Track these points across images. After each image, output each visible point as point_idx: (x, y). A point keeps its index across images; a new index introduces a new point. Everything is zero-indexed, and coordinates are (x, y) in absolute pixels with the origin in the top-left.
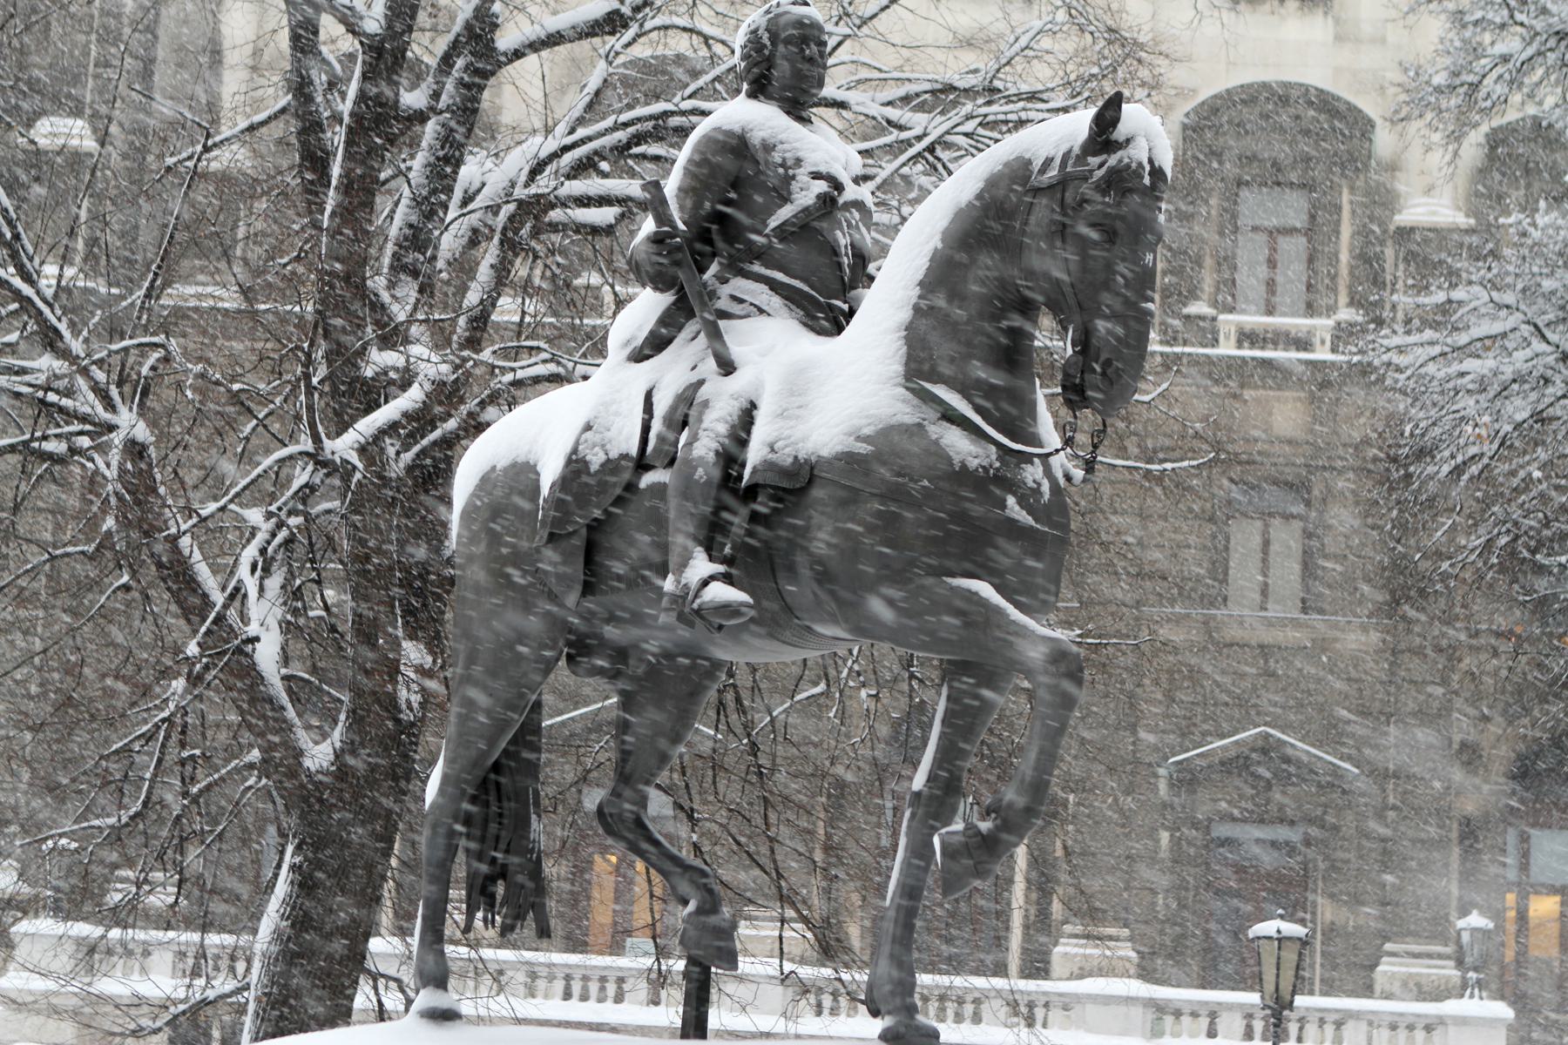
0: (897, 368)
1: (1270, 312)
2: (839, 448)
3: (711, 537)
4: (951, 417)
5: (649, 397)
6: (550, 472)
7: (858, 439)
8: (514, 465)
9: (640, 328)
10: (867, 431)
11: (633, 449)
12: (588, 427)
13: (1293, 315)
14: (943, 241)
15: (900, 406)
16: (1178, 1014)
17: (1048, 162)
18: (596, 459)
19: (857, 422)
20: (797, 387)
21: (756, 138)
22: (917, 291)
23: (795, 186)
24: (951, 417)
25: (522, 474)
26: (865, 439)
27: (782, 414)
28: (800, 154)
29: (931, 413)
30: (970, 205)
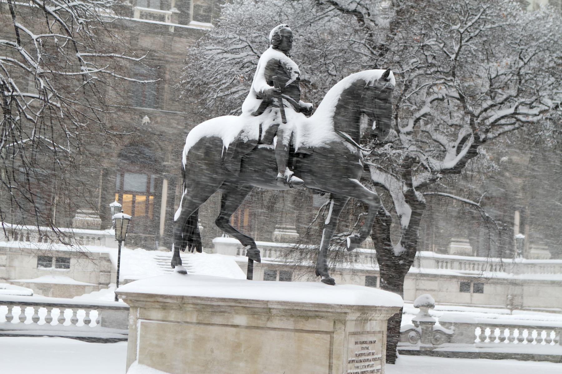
0: (332, 127)
1: (148, 6)
2: (321, 146)
3: (289, 164)
4: (347, 140)
5: (261, 125)
6: (227, 142)
7: (326, 144)
8: (213, 137)
9: (254, 107)
10: (328, 142)
11: (257, 138)
12: (242, 131)
13: (155, 8)
14: (341, 96)
15: (335, 137)
16: (465, 263)
17: (370, 83)
18: (246, 140)
19: (324, 140)
20: (306, 129)
21: (282, 61)
22: (335, 109)
23: (292, 75)
24: (347, 140)
25: (216, 141)
26: (328, 144)
27: (304, 136)
28: (292, 67)
29: (344, 140)
30: (348, 89)
